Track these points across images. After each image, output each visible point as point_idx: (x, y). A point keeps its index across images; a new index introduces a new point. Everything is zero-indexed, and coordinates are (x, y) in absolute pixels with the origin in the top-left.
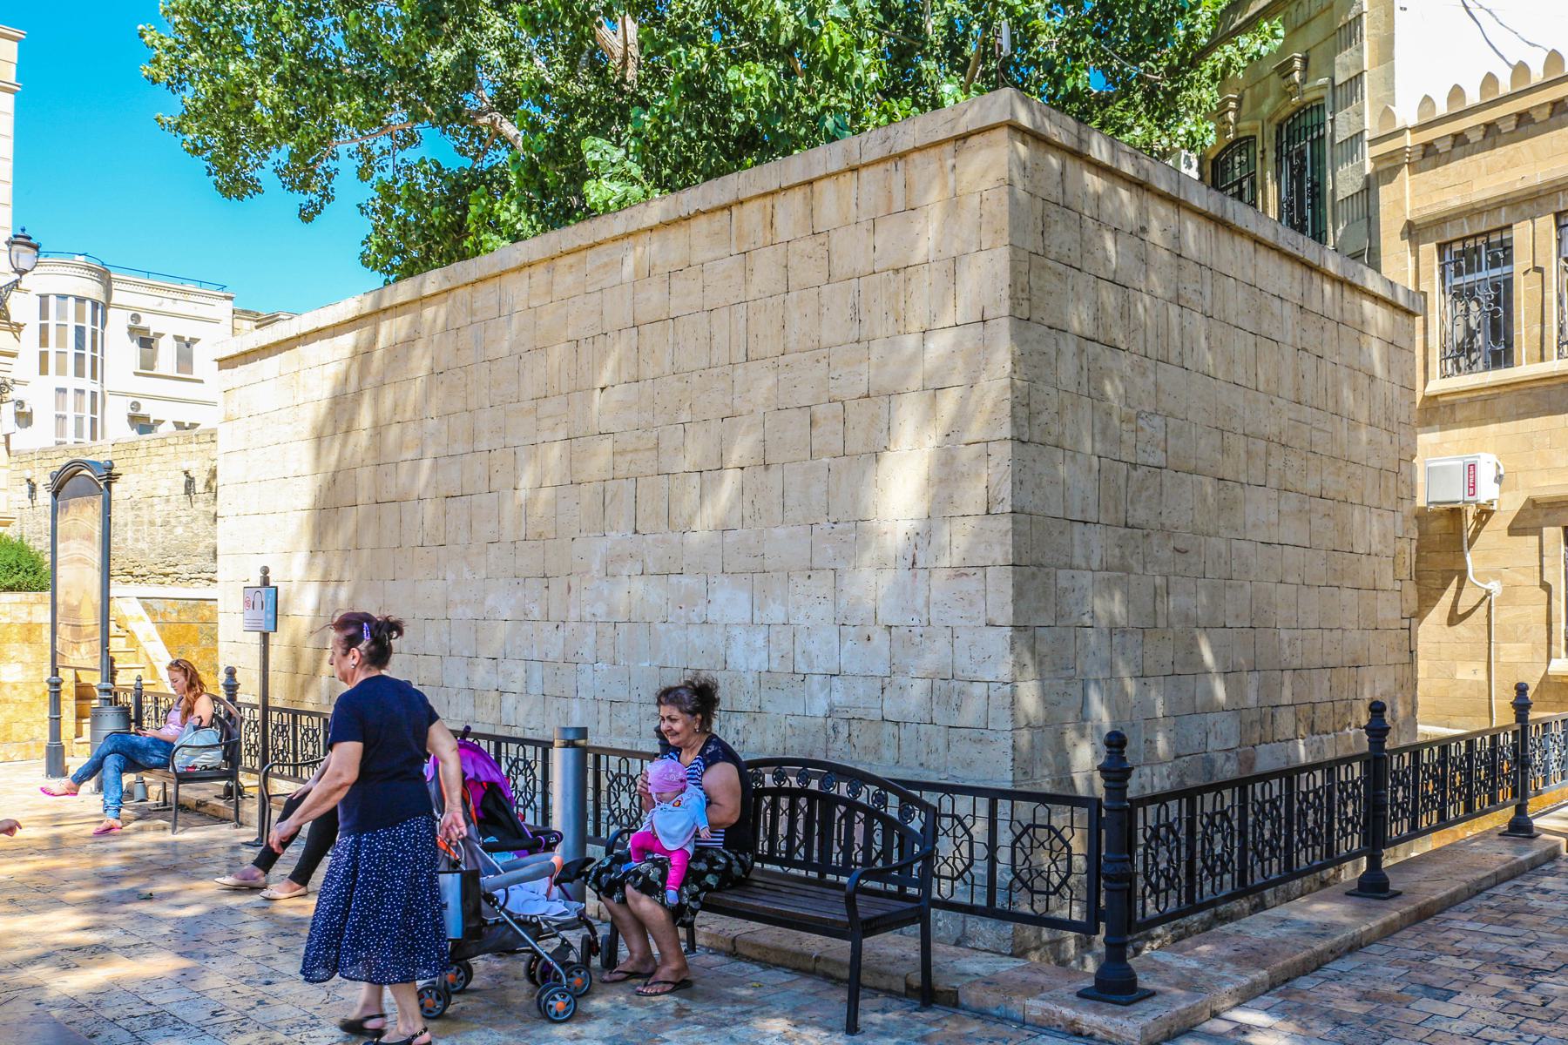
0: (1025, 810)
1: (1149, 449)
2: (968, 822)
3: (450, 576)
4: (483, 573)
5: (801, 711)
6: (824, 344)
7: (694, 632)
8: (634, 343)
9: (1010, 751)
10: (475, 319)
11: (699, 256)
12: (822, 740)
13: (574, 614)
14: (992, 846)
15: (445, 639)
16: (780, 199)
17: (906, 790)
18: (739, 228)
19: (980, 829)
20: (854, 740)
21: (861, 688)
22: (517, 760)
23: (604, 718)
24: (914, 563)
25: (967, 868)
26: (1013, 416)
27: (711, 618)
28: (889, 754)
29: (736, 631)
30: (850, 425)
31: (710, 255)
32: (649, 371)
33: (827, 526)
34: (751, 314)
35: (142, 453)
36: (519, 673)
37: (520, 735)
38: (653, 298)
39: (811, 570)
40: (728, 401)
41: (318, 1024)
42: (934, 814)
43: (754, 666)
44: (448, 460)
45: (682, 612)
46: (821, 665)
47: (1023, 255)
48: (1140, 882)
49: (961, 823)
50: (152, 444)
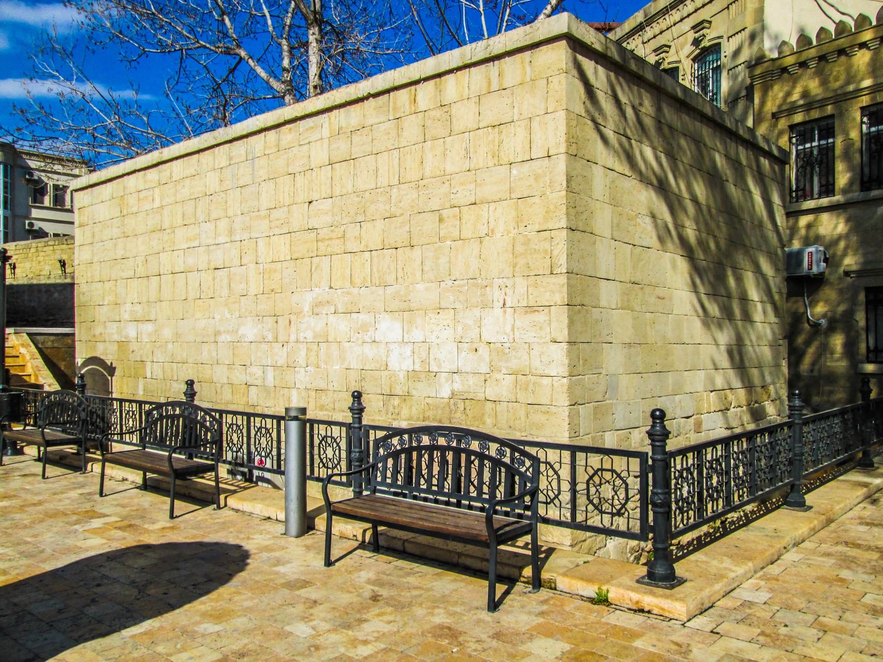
0: (595, 460)
1: (643, 236)
2: (557, 466)
3: (217, 317)
4: (237, 314)
5: (434, 395)
6: (447, 172)
7: (367, 347)
8: (329, 175)
9: (567, 418)
10: (232, 162)
11: (370, 121)
12: (447, 410)
13: (293, 338)
14: (573, 483)
15: (214, 354)
16: (418, 87)
17: (515, 446)
18: (395, 103)
19: (565, 473)
20: (468, 411)
21: (471, 381)
22: (261, 428)
23: (312, 400)
24: (504, 304)
25: (556, 496)
26: (567, 214)
27: (377, 340)
28: (489, 421)
29: (392, 346)
30: (464, 221)
31: (377, 121)
32: (337, 191)
33: (450, 283)
34: (402, 156)
35: (33, 250)
36: (259, 373)
37: (260, 412)
38: (342, 147)
39: (440, 309)
40: (388, 208)
41: (132, 617)
42: (535, 460)
43: (405, 368)
44: (215, 247)
45: (360, 336)
46: (447, 367)
47: (573, 116)
48: (674, 506)
49: (552, 467)
50: (40, 245)
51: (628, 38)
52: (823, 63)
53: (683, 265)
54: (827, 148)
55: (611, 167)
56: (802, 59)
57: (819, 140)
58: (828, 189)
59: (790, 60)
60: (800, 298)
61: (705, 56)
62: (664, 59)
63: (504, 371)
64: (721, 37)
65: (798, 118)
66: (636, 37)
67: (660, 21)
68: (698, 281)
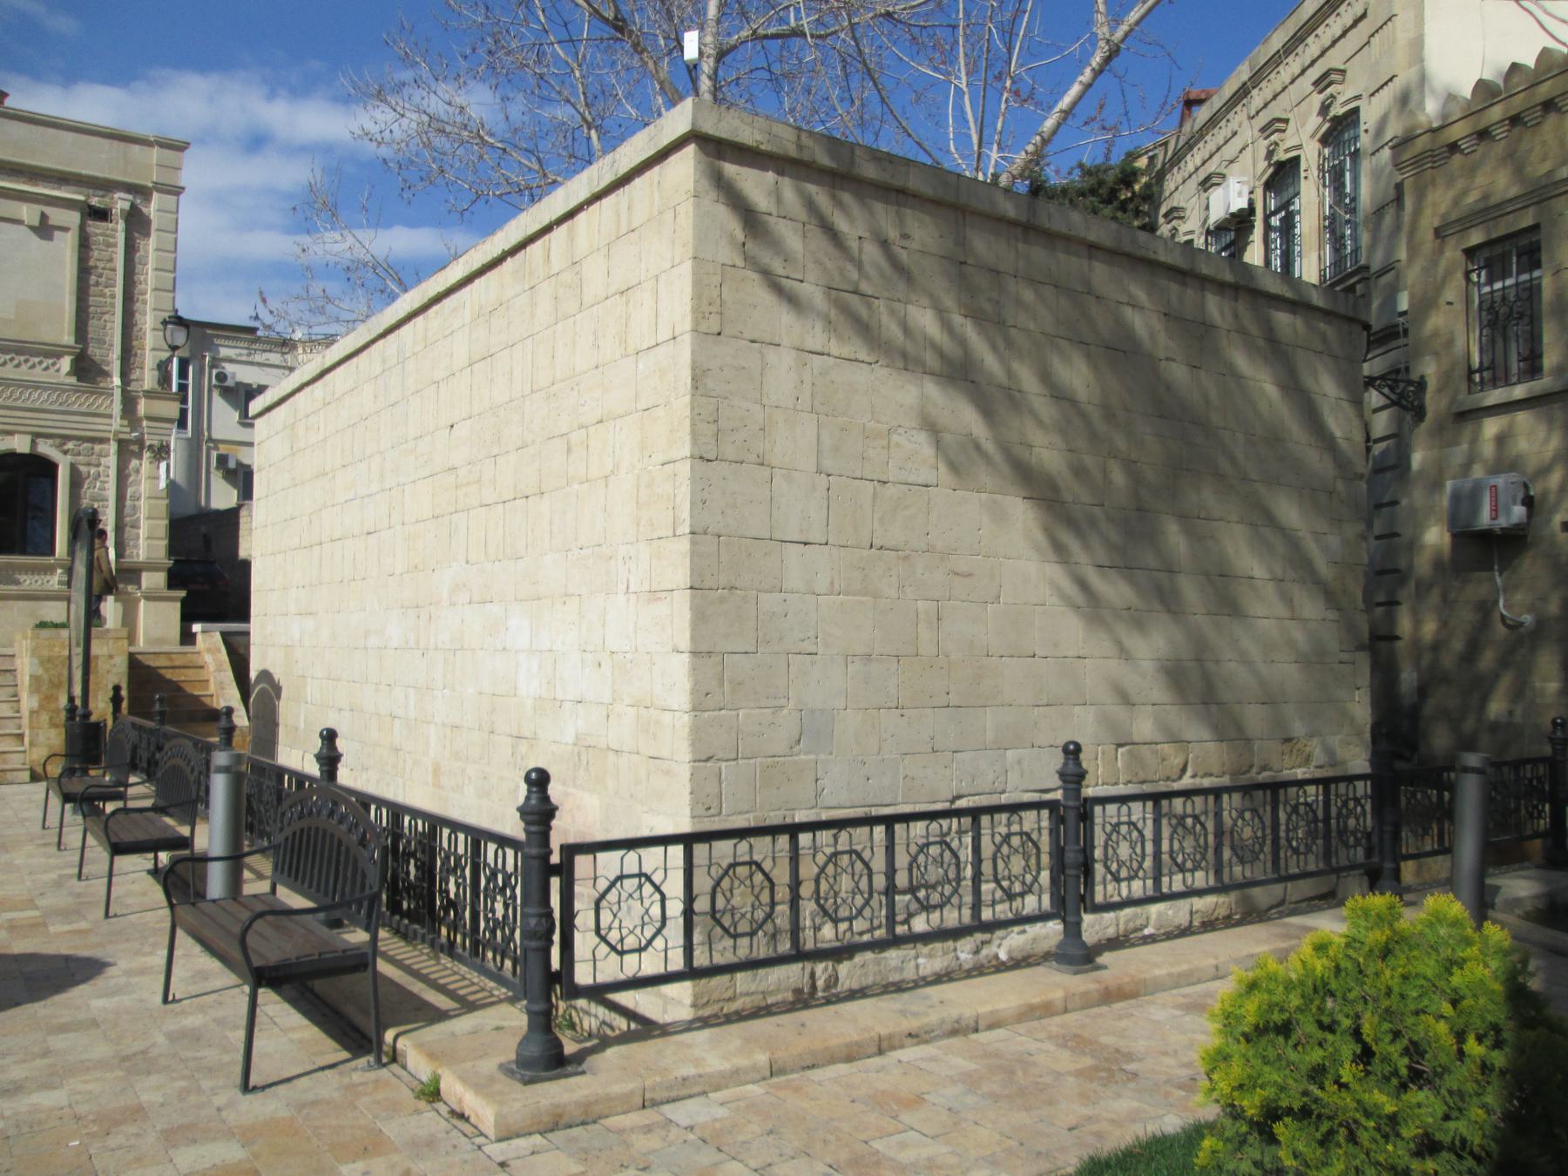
51: (1228, 111)
52: (1516, 130)
53: (1021, 513)
54: (1530, 289)
55: (819, 348)
56: (1482, 125)
57: (1518, 274)
58: (1533, 366)
59: (1457, 132)
60: (1484, 574)
61: (1342, 132)
62: (1276, 144)
63: (627, 701)
64: (1358, 97)
65: (1476, 238)
66: (1238, 108)
67: (1272, 76)
68: (1074, 544)
